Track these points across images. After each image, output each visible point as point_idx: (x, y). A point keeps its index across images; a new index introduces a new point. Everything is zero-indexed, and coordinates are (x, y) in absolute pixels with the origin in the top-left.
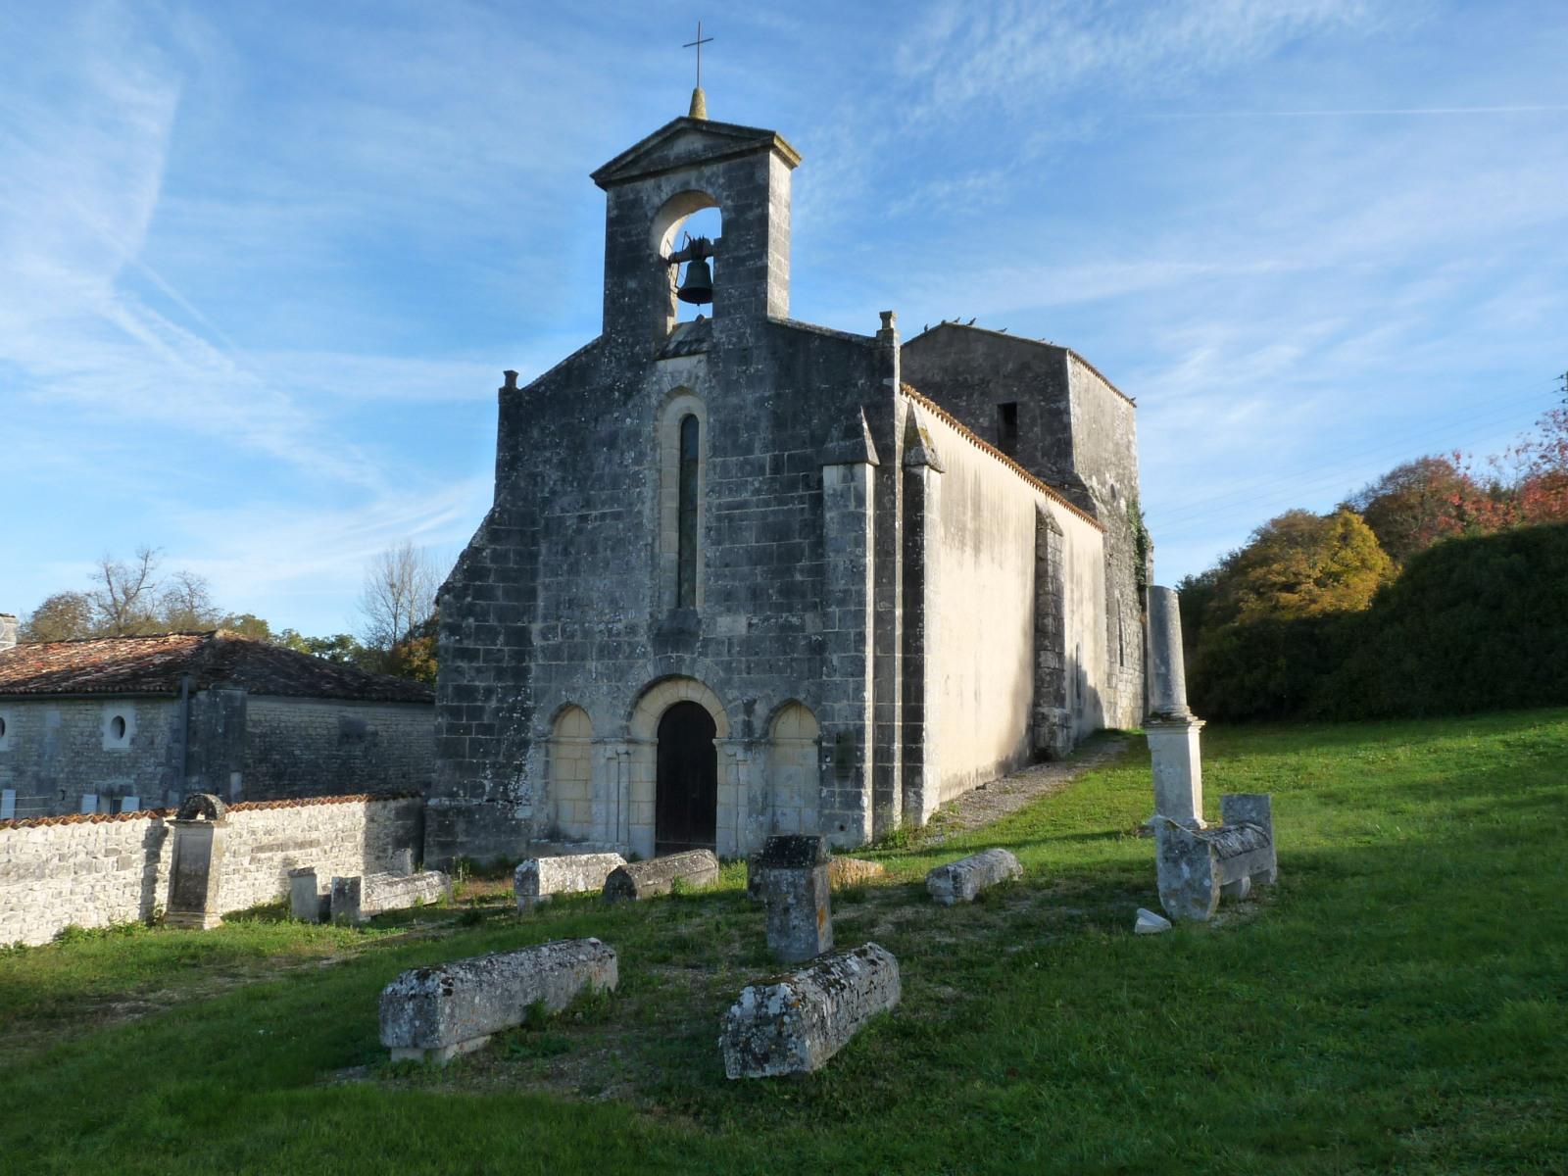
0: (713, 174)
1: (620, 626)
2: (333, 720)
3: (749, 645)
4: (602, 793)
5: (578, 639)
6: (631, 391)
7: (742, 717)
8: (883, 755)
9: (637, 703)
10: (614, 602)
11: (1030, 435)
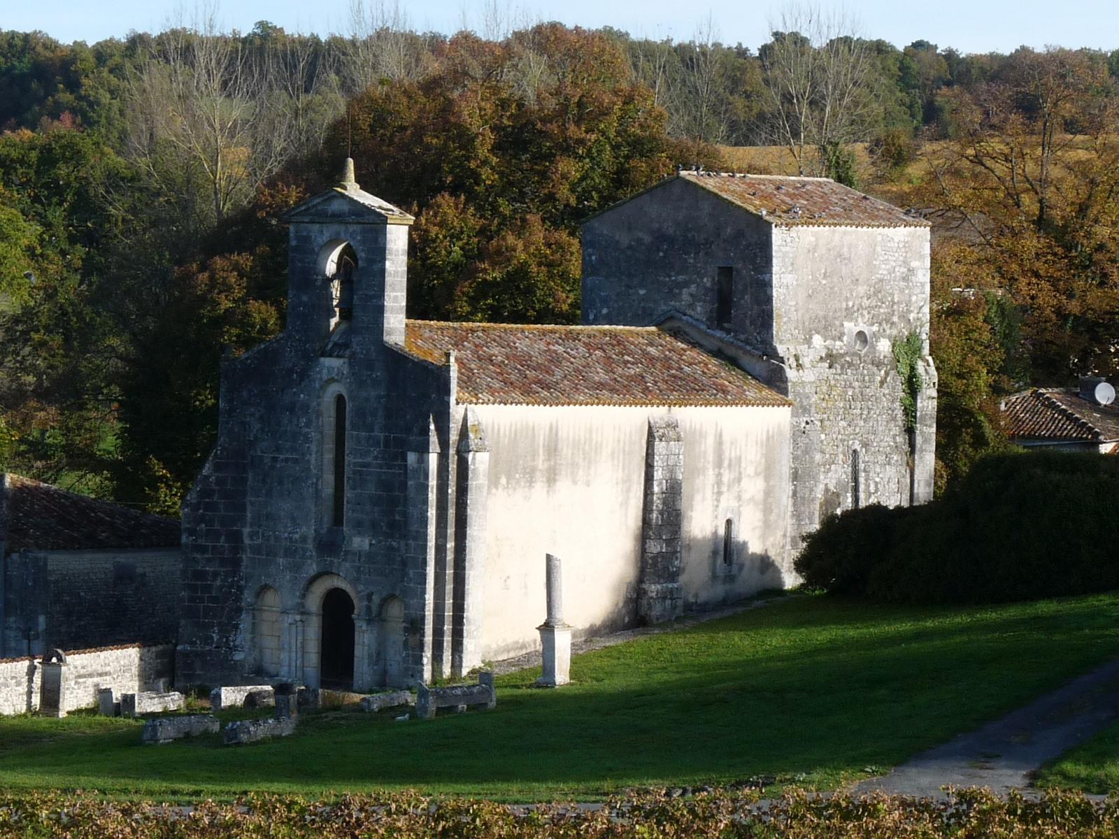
0: (354, 231)
1: (297, 536)
2: (109, 566)
3: (370, 557)
4: (286, 646)
5: (272, 541)
6: (304, 375)
7: (365, 603)
8: (438, 633)
9: (308, 588)
10: (293, 519)
11: (742, 302)
